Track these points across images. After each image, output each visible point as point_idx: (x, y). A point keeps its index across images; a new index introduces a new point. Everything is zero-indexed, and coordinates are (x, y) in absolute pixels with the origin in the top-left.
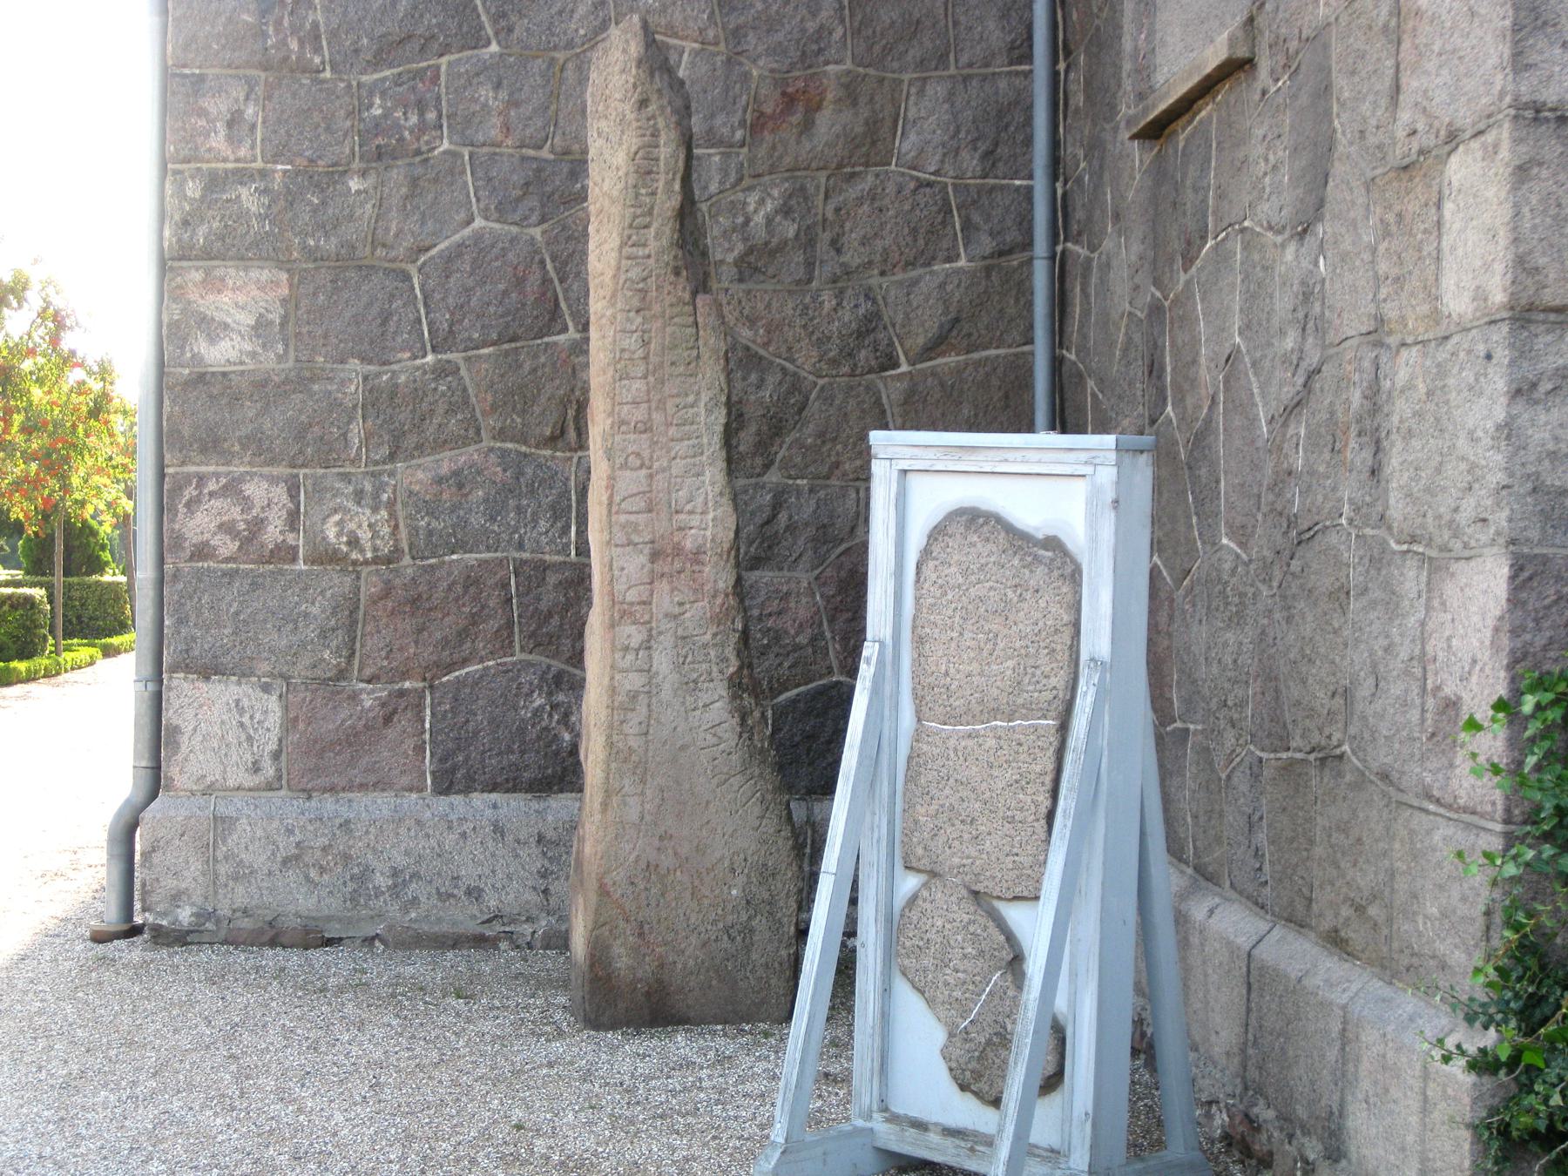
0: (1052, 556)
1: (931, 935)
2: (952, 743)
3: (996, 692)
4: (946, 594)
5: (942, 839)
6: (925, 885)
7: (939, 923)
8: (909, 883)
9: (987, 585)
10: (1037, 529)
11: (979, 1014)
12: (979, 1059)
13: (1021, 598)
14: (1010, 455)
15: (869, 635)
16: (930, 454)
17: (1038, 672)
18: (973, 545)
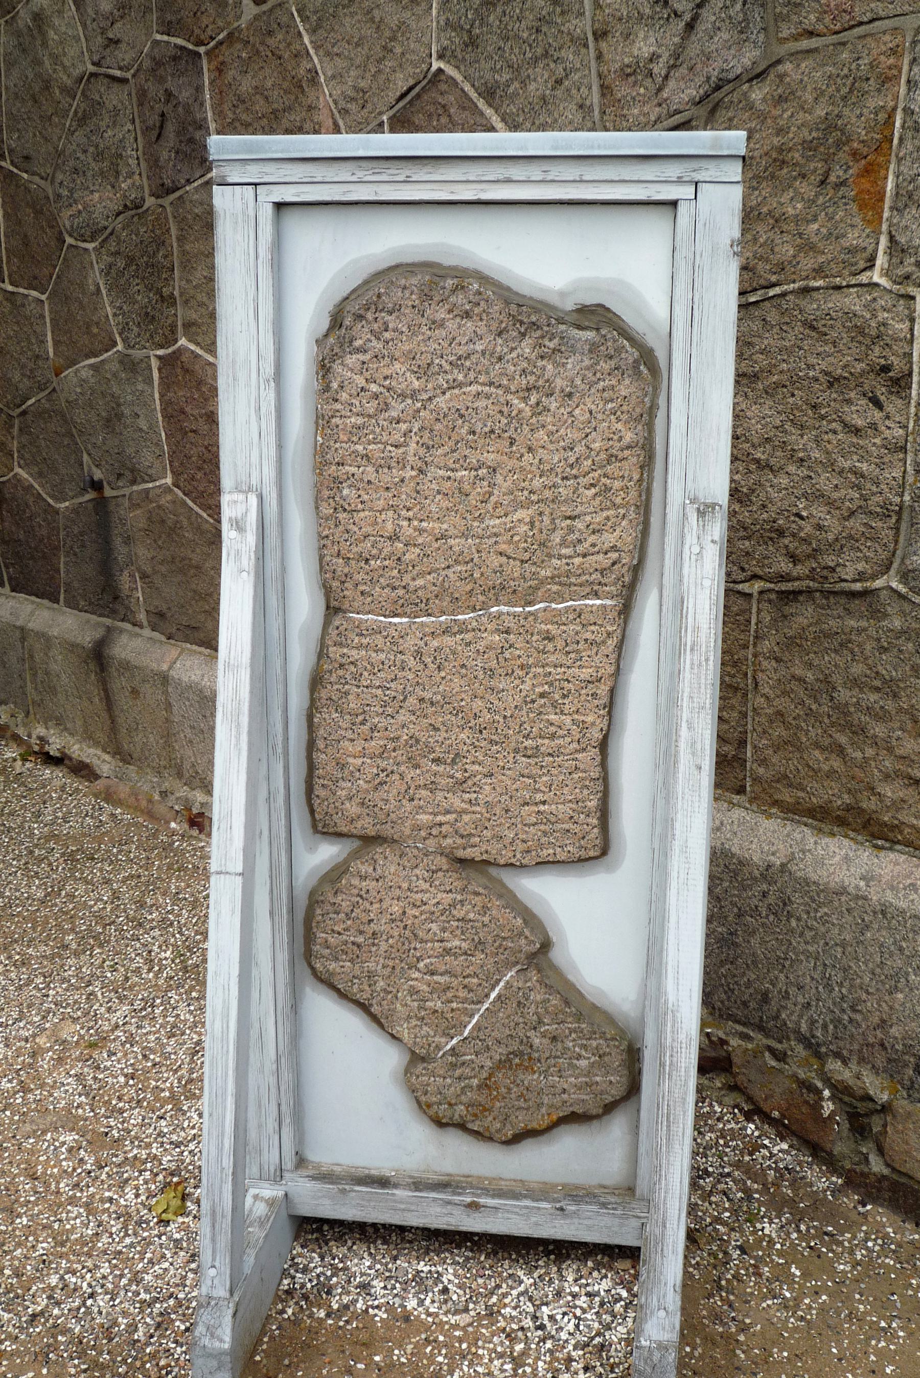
0: (609, 343)
1: (382, 926)
2: (410, 643)
3: (496, 561)
4: (387, 407)
5: (397, 786)
6: (355, 855)
7: (396, 909)
8: (327, 853)
9: (474, 388)
10: (562, 294)
11: (478, 1028)
12: (484, 1086)
13: (539, 409)
14: (517, 172)
15: (227, 480)
16: (343, 173)
17: (579, 524)
18: (437, 324)
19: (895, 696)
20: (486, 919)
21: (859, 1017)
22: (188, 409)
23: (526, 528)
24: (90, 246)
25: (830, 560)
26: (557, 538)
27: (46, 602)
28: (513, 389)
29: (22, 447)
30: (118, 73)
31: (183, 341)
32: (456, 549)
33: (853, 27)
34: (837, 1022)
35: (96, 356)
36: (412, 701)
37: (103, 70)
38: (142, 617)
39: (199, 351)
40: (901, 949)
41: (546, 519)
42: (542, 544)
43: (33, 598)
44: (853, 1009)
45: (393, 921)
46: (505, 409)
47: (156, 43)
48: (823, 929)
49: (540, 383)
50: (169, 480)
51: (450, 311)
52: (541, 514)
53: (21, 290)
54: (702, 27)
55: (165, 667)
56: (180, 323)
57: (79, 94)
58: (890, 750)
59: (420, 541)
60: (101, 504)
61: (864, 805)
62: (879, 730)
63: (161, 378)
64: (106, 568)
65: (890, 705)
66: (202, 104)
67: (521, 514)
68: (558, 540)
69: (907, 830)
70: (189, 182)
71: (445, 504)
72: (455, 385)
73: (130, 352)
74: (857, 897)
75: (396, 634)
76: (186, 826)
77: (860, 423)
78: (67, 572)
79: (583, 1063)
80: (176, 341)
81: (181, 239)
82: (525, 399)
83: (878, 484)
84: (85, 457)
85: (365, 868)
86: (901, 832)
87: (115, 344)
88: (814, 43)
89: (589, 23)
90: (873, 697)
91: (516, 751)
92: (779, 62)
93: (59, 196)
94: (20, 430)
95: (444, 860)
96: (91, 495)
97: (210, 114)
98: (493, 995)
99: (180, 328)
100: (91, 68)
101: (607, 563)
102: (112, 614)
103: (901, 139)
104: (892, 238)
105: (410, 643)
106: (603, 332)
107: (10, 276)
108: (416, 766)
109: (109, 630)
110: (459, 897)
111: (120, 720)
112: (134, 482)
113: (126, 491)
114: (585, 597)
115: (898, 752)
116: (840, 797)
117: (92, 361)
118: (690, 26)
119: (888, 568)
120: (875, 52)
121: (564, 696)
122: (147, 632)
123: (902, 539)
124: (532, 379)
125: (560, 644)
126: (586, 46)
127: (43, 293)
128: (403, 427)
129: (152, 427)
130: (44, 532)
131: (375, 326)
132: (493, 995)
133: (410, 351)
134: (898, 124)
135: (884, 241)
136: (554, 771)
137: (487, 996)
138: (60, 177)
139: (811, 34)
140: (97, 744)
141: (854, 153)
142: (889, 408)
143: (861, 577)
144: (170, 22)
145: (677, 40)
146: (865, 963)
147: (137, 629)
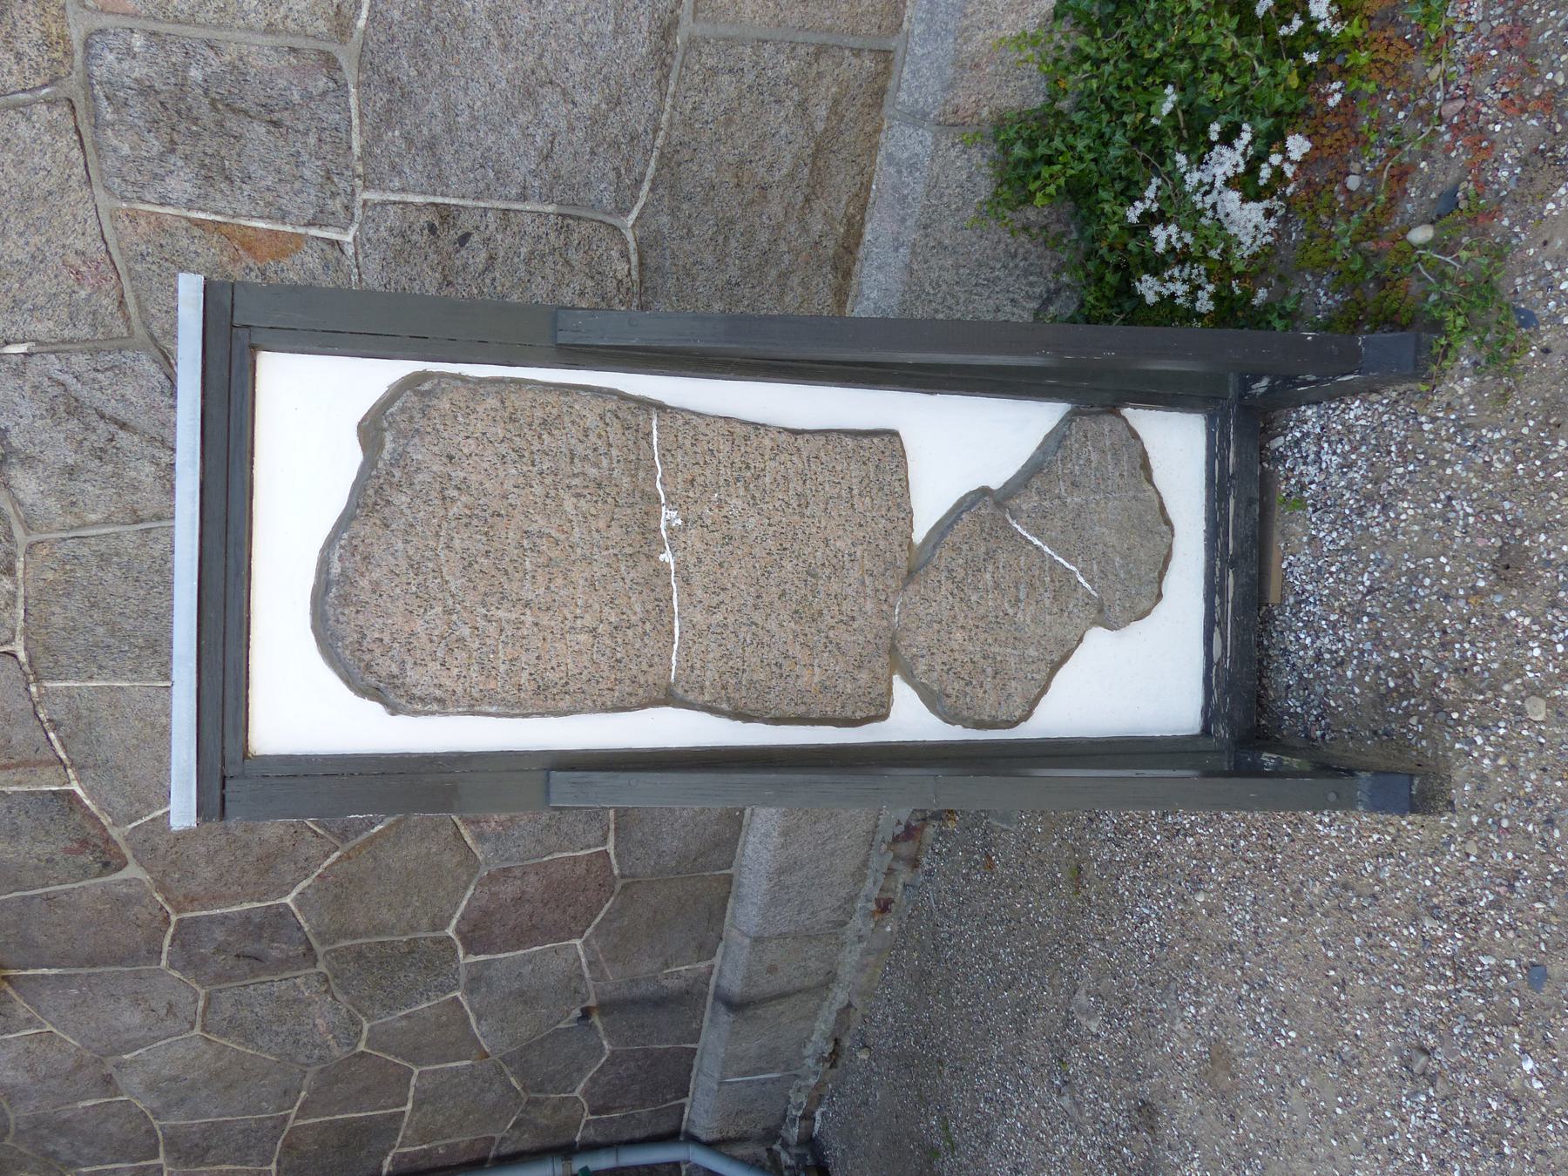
2: (699, 618)
3: (616, 530)
4: (461, 639)
18: (376, 587)
19: (731, 222)
20: (965, 547)
21: (1021, 251)
22: (511, 923)
23: (582, 501)
24: (366, 1026)
25: (611, 285)
26: (593, 472)
27: (696, 1062)
28: (442, 512)
29: (556, 1090)
30: (201, 1003)
31: (450, 932)
32: (605, 571)
33: (113, 262)
34: (1027, 273)
35: (467, 1017)
36: (758, 617)
37: (199, 1019)
38: (703, 965)
39: (458, 915)
40: (958, 210)
41: (575, 482)
42: (599, 486)
43: (693, 1074)
44: (1014, 256)
45: (971, 639)
46: (465, 520)
47: (172, 966)
48: (944, 287)
49: (438, 486)
50: (578, 942)
51: (362, 575)
52: (569, 487)
53: (411, 1094)
54: (123, 414)
55: (747, 941)
56: (432, 935)
57: (223, 1042)
58: (780, 226)
59: (597, 606)
60: (605, 1008)
61: (831, 252)
62: (763, 237)
63: (484, 953)
64: (660, 1002)
65: (740, 227)
66: (226, 917)
67: (569, 505)
68: (594, 471)
69: (851, 210)
70: (300, 928)
71: (559, 581)
72: (438, 571)
73: (462, 982)
74: (914, 253)
75: (691, 632)
76: (888, 916)
77: (483, 255)
78: (667, 1041)
79: (1094, 457)
80: (449, 938)
81: (355, 935)
82: (453, 500)
83: (540, 237)
84: (561, 1026)
85: (922, 666)
86: (854, 216)
87: (456, 999)
88: (130, 299)
89: (127, 528)
90: (733, 243)
91: (802, 515)
92: (152, 336)
93: (321, 1058)
94: (540, 1091)
95: (910, 587)
96: (596, 1019)
97: (235, 909)
98: (1037, 542)
99: (437, 934)
100: (197, 1031)
101: (616, 424)
102: (703, 995)
103: (216, 213)
104: (309, 224)
105: (699, 618)
106: (386, 425)
107: (398, 1106)
108: (820, 613)
109: (717, 997)
110: (945, 574)
111: (797, 984)
112: (581, 977)
113: (590, 984)
114: (650, 445)
115: (782, 218)
116: (825, 276)
117: (473, 1020)
118: (123, 426)
119: (615, 228)
120: (135, 239)
121: (748, 467)
122: (717, 960)
123: (590, 215)
124: (434, 494)
125: (697, 470)
126: (148, 531)
127: (412, 1072)
128: (481, 623)
129: (529, 959)
130: (632, 1064)
131: (378, 652)
132: (1037, 542)
133: (404, 616)
134: (202, 216)
135: (314, 232)
136: (820, 479)
137: (1037, 548)
138: (302, 1059)
139: (122, 303)
140: (819, 1007)
141: (234, 261)
142: (469, 227)
143: (625, 255)
144: (149, 952)
145: (136, 439)
146: (972, 245)
147: (715, 971)
